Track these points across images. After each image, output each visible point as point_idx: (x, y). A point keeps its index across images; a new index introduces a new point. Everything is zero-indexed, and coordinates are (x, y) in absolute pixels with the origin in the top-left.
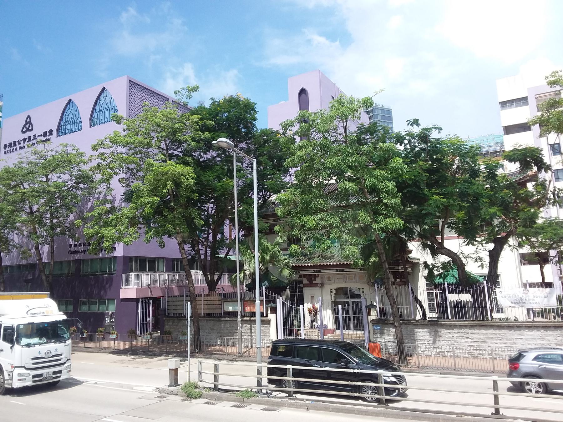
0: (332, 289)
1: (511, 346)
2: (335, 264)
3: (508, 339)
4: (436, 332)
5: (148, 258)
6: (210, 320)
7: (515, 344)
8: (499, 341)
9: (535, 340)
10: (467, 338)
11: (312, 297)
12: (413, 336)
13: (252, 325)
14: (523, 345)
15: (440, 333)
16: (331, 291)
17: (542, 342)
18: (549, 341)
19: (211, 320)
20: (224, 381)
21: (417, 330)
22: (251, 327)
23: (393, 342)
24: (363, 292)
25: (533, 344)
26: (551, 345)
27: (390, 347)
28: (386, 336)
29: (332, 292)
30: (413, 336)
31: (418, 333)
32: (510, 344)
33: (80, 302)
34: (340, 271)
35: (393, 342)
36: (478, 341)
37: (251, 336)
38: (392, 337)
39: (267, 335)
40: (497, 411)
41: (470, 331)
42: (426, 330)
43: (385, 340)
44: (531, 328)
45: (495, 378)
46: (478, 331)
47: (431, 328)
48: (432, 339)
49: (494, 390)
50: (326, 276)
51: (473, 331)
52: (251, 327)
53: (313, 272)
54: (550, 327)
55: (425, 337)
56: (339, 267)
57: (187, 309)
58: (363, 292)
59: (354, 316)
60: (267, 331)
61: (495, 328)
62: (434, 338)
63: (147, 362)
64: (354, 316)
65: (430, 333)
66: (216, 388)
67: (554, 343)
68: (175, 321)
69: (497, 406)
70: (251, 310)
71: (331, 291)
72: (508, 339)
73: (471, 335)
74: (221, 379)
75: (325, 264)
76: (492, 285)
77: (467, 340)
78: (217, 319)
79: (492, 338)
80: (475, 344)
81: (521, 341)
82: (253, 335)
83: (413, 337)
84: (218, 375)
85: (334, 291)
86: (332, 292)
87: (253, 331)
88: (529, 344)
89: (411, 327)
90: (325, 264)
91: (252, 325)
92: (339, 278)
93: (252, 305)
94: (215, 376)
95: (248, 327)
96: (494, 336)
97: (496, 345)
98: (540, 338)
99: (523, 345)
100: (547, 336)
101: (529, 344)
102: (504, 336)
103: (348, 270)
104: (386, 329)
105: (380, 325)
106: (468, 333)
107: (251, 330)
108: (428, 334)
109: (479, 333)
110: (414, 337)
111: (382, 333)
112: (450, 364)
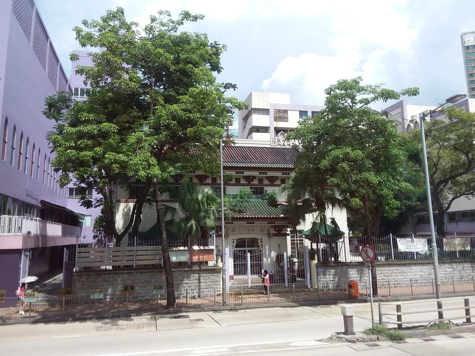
0: (233, 240)
1: (406, 277)
2: (251, 217)
3: (404, 273)
4: (362, 271)
5: (428, 213)
6: (146, 272)
7: (408, 275)
8: (399, 274)
9: (417, 273)
10: (381, 274)
11: (278, 245)
12: (347, 274)
13: (201, 275)
14: (412, 276)
15: (364, 271)
16: (233, 241)
17: (421, 274)
18: (425, 272)
19: (148, 272)
20: (407, 320)
21: (350, 270)
22: (199, 277)
23: (332, 281)
24: (261, 242)
25: (417, 276)
26: (426, 275)
27: (330, 285)
28: (327, 276)
29: (233, 242)
30: (347, 274)
31: (351, 273)
32: (405, 276)
33: (459, 253)
34: (250, 223)
35: (332, 281)
36: (388, 275)
37: (199, 286)
38: (332, 277)
39: (218, 283)
40: (468, 320)
41: (382, 269)
42: (356, 269)
43: (327, 280)
44: (416, 265)
45: (467, 297)
46: (387, 269)
47: (359, 267)
48: (359, 276)
49: (398, 311)
50: (231, 228)
51: (385, 269)
52: (199, 277)
53: (247, 224)
54: (425, 263)
55: (355, 275)
56: (251, 220)
57: (304, 258)
58: (261, 242)
59: (235, 263)
60: (217, 279)
61: (426, 264)
62: (360, 275)
63: (289, 315)
64: (235, 263)
65: (358, 271)
66: (400, 327)
67: (427, 273)
68: (91, 276)
69: (468, 317)
70: (199, 259)
71: (233, 241)
72: (404, 273)
73: (383, 272)
74: (405, 318)
75: (242, 217)
76: (441, 237)
77: (381, 275)
78: (157, 270)
79: (395, 273)
80: (386, 278)
81: (410, 274)
82: (201, 284)
83: (346, 275)
84: (442, 311)
85: (235, 242)
86: (233, 242)
87: (202, 281)
88: (415, 275)
89: (345, 268)
90: (242, 217)
91: (201, 275)
92: (243, 230)
93: (200, 254)
94: (439, 312)
95: (196, 276)
96: (396, 271)
97: (398, 277)
98: (420, 271)
99: (412, 276)
100: (424, 270)
101: (415, 275)
102: (402, 271)
103: (257, 223)
104: (327, 270)
105: (324, 267)
106: (381, 270)
107: (199, 279)
108: (357, 272)
109: (388, 270)
110: (348, 275)
111: (324, 274)
112: (387, 294)
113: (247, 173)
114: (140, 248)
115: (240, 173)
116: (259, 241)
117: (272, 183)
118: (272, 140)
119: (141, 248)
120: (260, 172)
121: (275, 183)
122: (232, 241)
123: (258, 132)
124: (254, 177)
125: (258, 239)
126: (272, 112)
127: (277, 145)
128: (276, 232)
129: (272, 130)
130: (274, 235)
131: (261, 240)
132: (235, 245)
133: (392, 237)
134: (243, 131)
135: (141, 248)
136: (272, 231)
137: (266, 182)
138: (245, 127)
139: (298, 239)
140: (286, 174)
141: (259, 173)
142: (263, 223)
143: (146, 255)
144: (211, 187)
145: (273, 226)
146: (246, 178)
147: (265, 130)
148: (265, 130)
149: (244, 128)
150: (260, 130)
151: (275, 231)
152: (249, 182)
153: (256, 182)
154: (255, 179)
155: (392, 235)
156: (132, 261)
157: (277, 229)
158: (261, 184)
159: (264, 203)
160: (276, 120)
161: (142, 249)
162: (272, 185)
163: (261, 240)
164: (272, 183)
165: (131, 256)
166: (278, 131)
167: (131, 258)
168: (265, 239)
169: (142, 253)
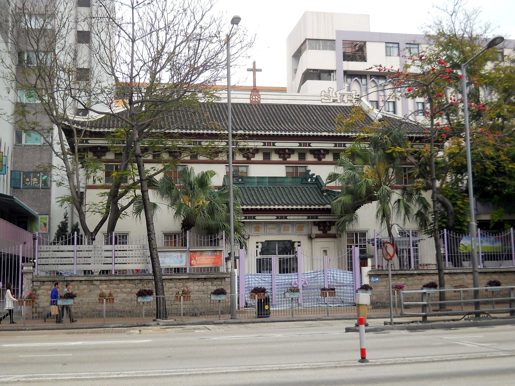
0: (257, 243)
11: (324, 251)
16: (257, 244)
29: (257, 247)
53: (276, 219)
71: (257, 244)
85: (260, 246)
113: (280, 145)
114: (120, 247)
115: (269, 144)
116: (296, 245)
117: (320, 159)
118: (323, 94)
119: (122, 247)
120: (274, 145)
121: (323, 160)
122: (256, 245)
123: (319, 78)
124: (292, 151)
125: (295, 242)
126: (339, 46)
127: (332, 101)
128: (321, 232)
129: (340, 75)
130: (318, 236)
131: (299, 244)
132: (259, 250)
133: (447, 235)
134: (293, 78)
135: (122, 247)
136: (315, 231)
137: (310, 158)
138: (295, 71)
139: (359, 244)
140: (340, 145)
141: (299, 144)
142: (300, 217)
143: (119, 251)
144: (286, 166)
145: (317, 223)
146: (279, 152)
147: (327, 74)
148: (327, 74)
149: (295, 73)
150: (322, 75)
151: (319, 230)
152: (285, 159)
153: (294, 158)
154: (293, 153)
155: (447, 231)
156: (110, 264)
157: (322, 228)
158: (267, 161)
159: (305, 189)
160: (347, 57)
161: (123, 249)
162: (320, 162)
163: (299, 244)
164: (320, 159)
165: (108, 257)
166: (349, 75)
167: (109, 260)
168: (304, 241)
169: (123, 254)
